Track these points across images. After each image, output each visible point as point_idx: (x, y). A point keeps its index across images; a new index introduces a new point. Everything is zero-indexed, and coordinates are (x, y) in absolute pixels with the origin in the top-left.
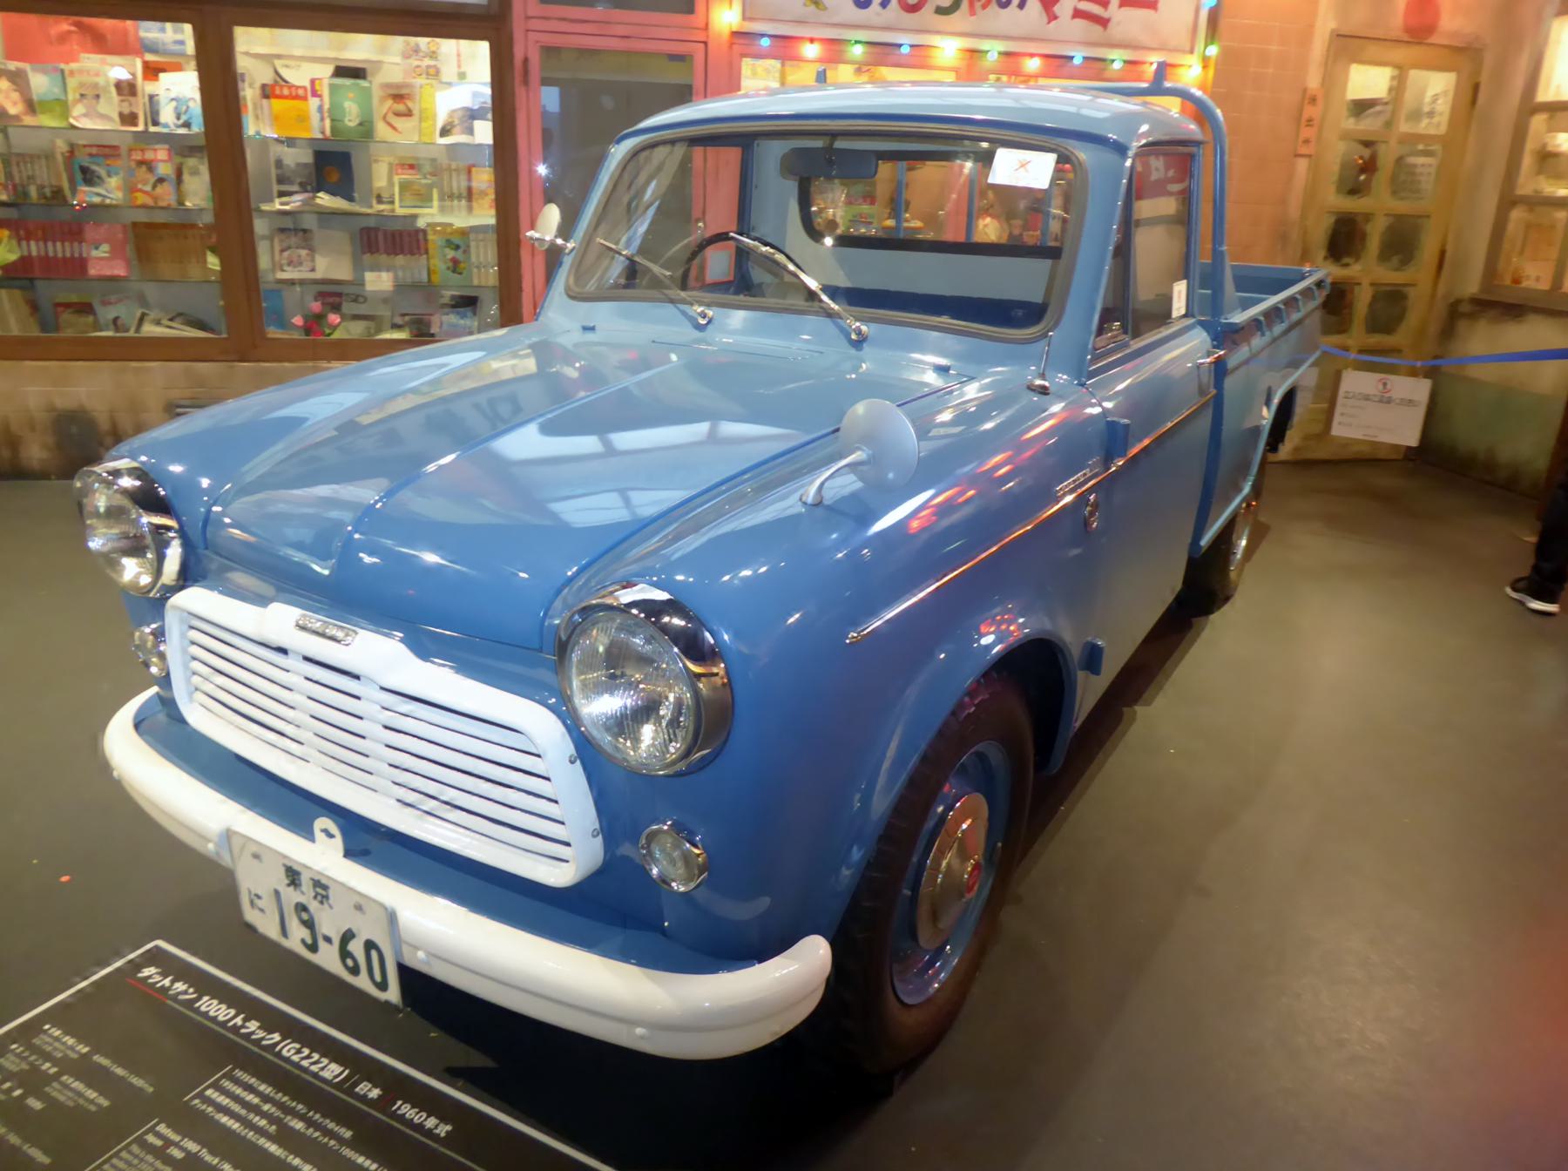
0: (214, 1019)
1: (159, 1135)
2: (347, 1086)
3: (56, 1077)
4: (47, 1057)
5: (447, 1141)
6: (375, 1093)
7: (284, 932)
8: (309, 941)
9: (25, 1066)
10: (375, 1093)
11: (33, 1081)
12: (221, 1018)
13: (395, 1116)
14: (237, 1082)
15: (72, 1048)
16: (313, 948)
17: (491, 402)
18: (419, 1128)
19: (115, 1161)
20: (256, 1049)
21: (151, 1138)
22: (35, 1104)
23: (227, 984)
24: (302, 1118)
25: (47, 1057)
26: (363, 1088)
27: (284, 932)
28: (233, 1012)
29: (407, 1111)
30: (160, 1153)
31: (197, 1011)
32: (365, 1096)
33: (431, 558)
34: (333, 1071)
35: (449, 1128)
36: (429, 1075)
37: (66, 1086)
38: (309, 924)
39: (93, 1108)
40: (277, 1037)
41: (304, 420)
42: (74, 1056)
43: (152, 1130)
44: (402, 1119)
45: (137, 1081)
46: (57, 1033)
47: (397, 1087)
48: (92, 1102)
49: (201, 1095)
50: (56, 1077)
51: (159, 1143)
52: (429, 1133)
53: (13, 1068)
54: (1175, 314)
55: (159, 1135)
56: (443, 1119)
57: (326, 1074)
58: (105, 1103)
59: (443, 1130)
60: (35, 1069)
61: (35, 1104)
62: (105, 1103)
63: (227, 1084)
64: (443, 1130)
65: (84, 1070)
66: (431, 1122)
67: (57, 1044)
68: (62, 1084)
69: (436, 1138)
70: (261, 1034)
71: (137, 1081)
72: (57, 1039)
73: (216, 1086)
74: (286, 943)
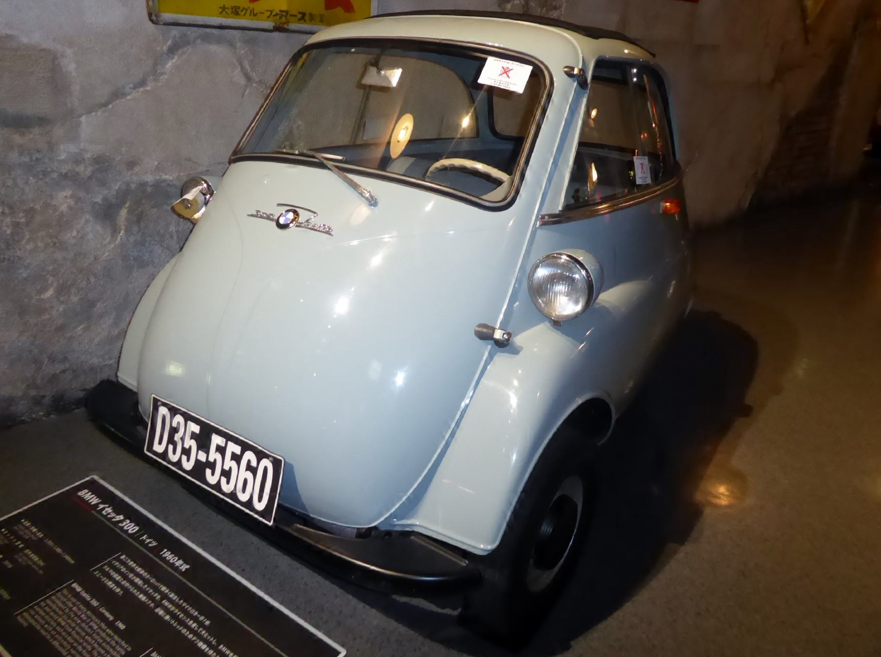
5: (185, 574)
6: (154, 544)
12: (130, 531)
14: (123, 563)
15: (34, 534)
17: (630, 193)
18: (172, 565)
19: (48, 601)
20: (107, 523)
29: (168, 555)
32: (173, 564)
33: (355, 243)
34: (131, 528)
35: (188, 567)
36: (193, 542)
42: (34, 538)
44: (164, 560)
45: (68, 558)
46: (35, 530)
48: (35, 563)
49: (101, 570)
50: (22, 549)
52: (176, 569)
56: (186, 562)
59: (185, 567)
64: (185, 567)
65: (37, 546)
68: (26, 555)
70: (113, 515)
71: (68, 558)
72: (27, 528)
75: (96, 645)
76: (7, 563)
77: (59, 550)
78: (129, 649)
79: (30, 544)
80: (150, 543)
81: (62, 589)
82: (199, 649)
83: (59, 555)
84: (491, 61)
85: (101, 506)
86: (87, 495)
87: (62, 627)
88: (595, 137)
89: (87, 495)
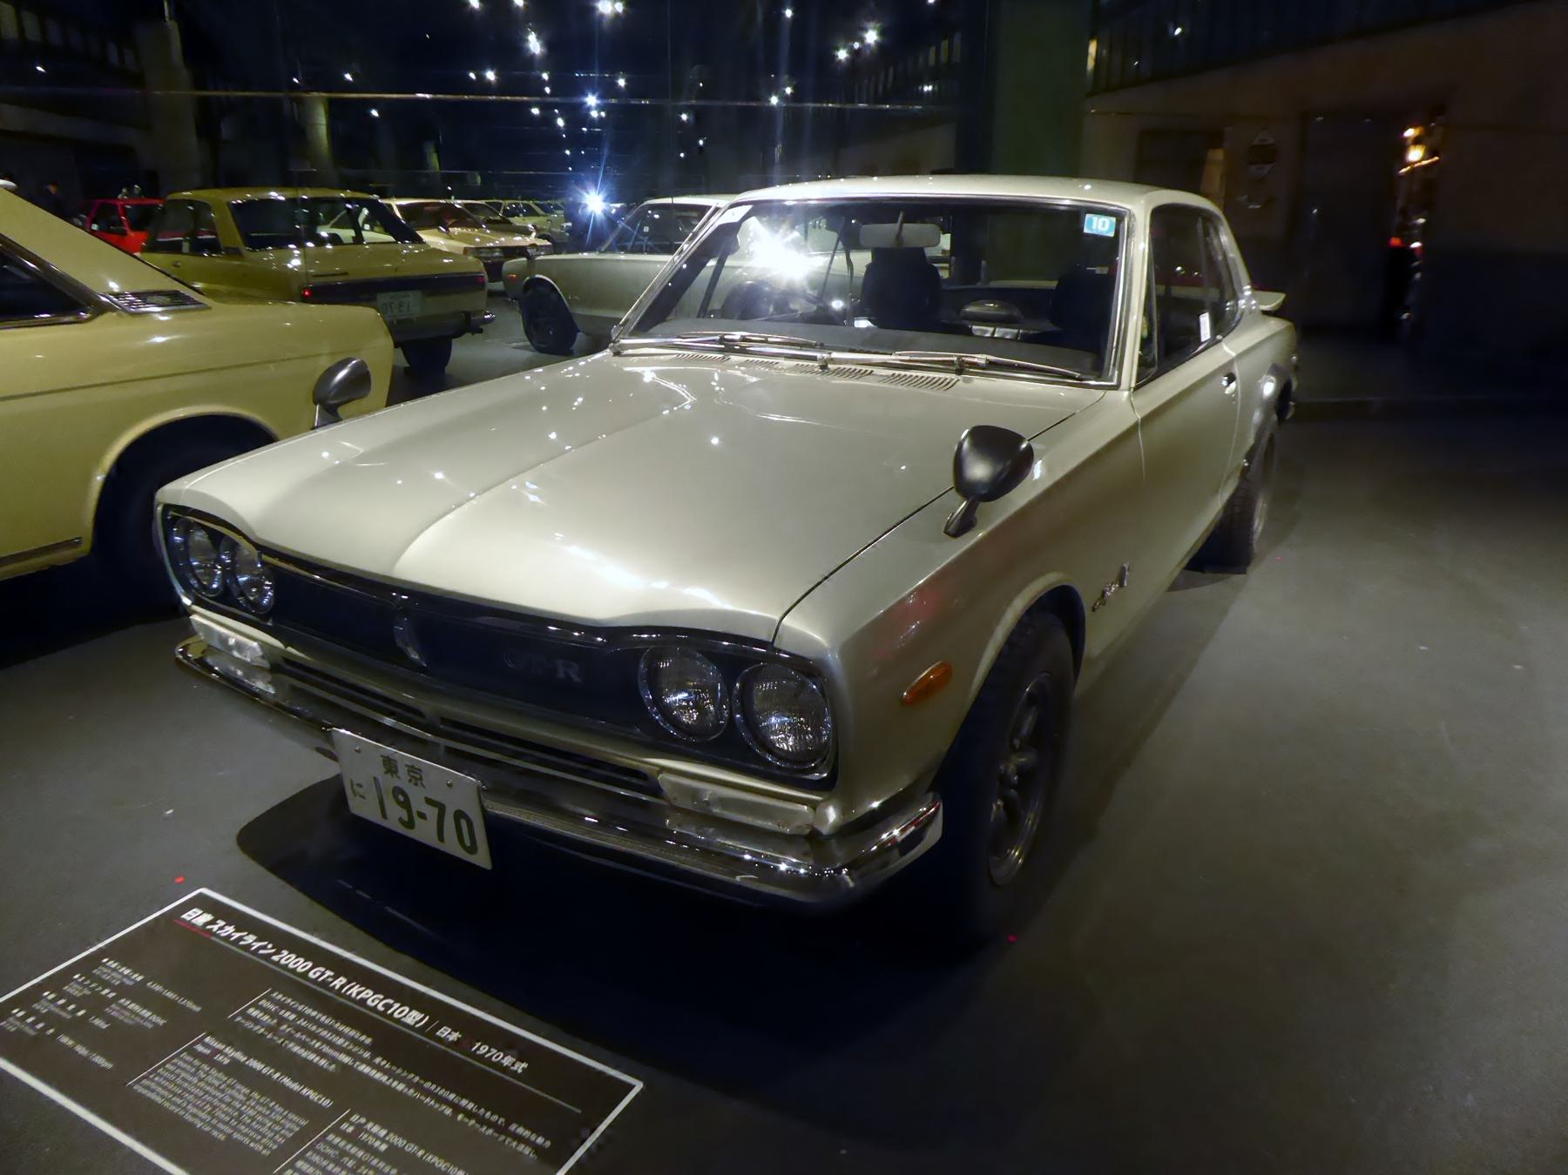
0: (294, 971)
1: (207, 1046)
2: (429, 1031)
3: (115, 999)
4: (106, 984)
6: (455, 1036)
7: (384, 816)
8: (406, 818)
9: (87, 992)
10: (455, 1036)
11: (96, 1005)
12: (299, 970)
13: (474, 1056)
16: (410, 824)
18: (498, 1066)
21: (200, 1048)
22: (100, 1023)
23: (230, 907)
24: (294, 1011)
25: (106, 984)
26: (444, 1032)
27: (384, 816)
28: (310, 964)
30: (209, 1060)
31: (349, 998)
34: (413, 1017)
35: (525, 1065)
37: (125, 1008)
38: (406, 804)
39: (150, 1026)
40: (343, 980)
41: (393, 400)
43: (201, 1041)
46: (127, 972)
47: (474, 1030)
48: (146, 1019)
50: (115, 999)
51: (208, 1052)
52: (505, 1070)
53: (77, 994)
54: (1203, 339)
55: (207, 1046)
57: (410, 1020)
58: (161, 1022)
59: (520, 1067)
60: (95, 994)
61: (100, 1023)
62: (161, 1022)
63: (263, 1003)
64: (520, 1067)
66: (507, 1061)
67: (278, 1118)
69: (515, 1074)
72: (114, 970)
73: (256, 1006)
74: (385, 824)
75: (216, 1102)
76: (98, 1022)
77: (170, 995)
78: (304, 1123)
79: (123, 991)
80: (241, 939)
81: (325, 1135)
82: (361, 1074)
83: (159, 993)
84: (1088, 216)
85: (238, 935)
86: (198, 918)
87: (175, 1094)
88: (942, 140)
89: (198, 918)
